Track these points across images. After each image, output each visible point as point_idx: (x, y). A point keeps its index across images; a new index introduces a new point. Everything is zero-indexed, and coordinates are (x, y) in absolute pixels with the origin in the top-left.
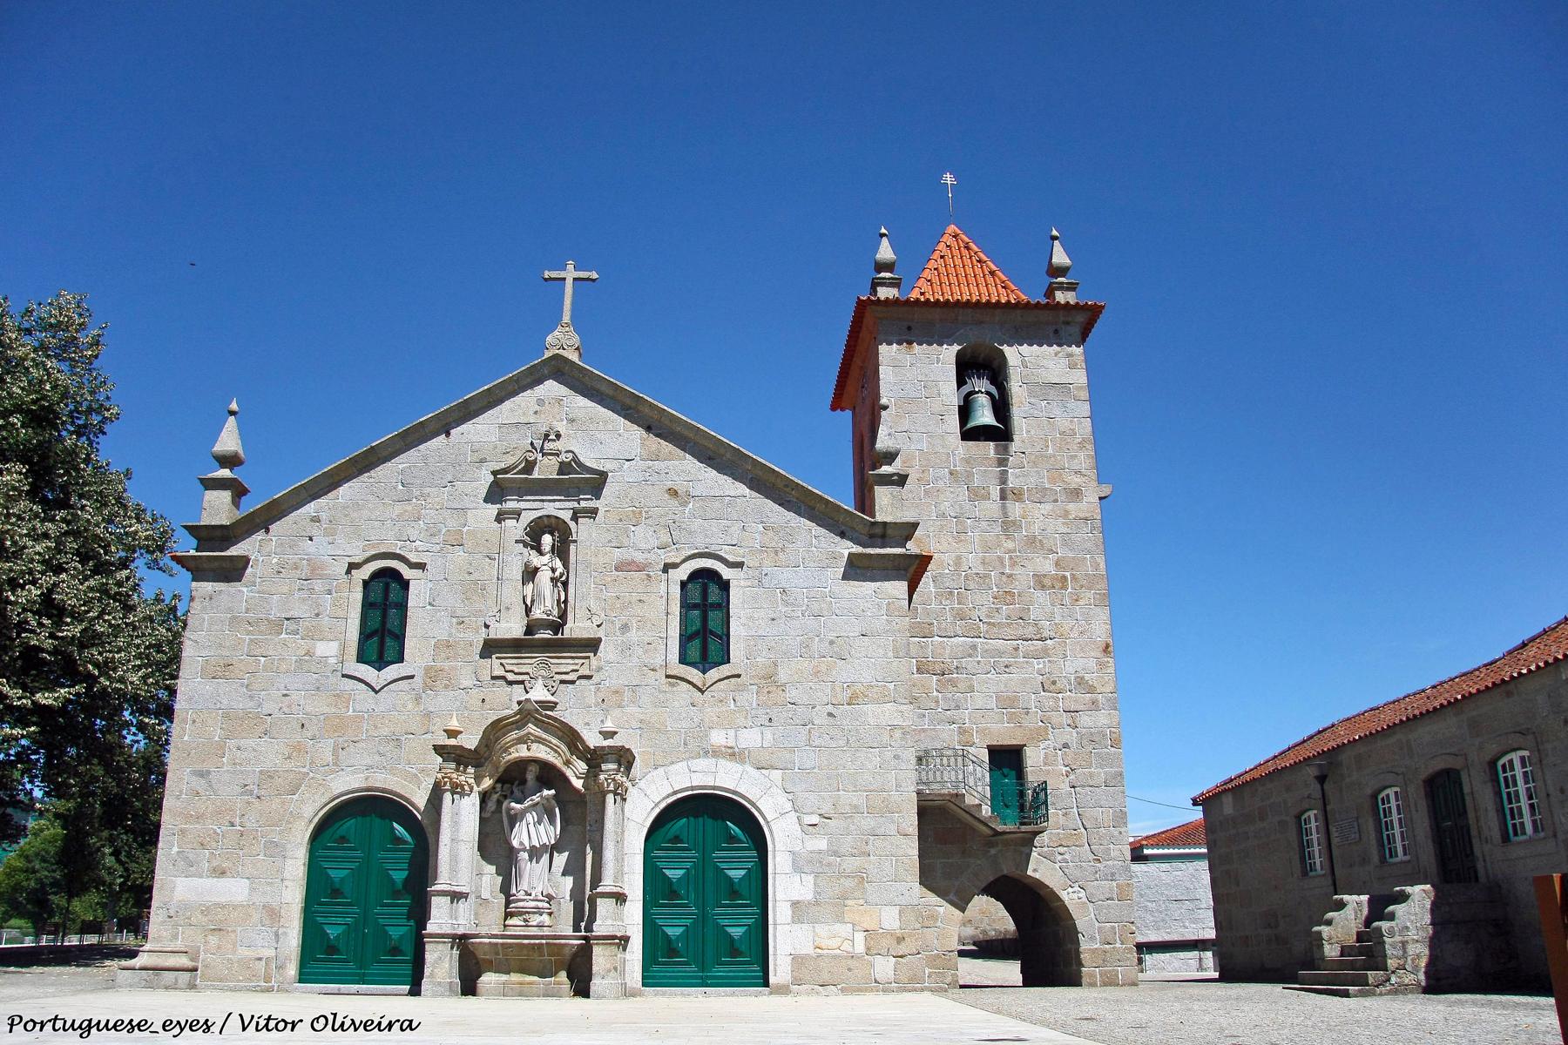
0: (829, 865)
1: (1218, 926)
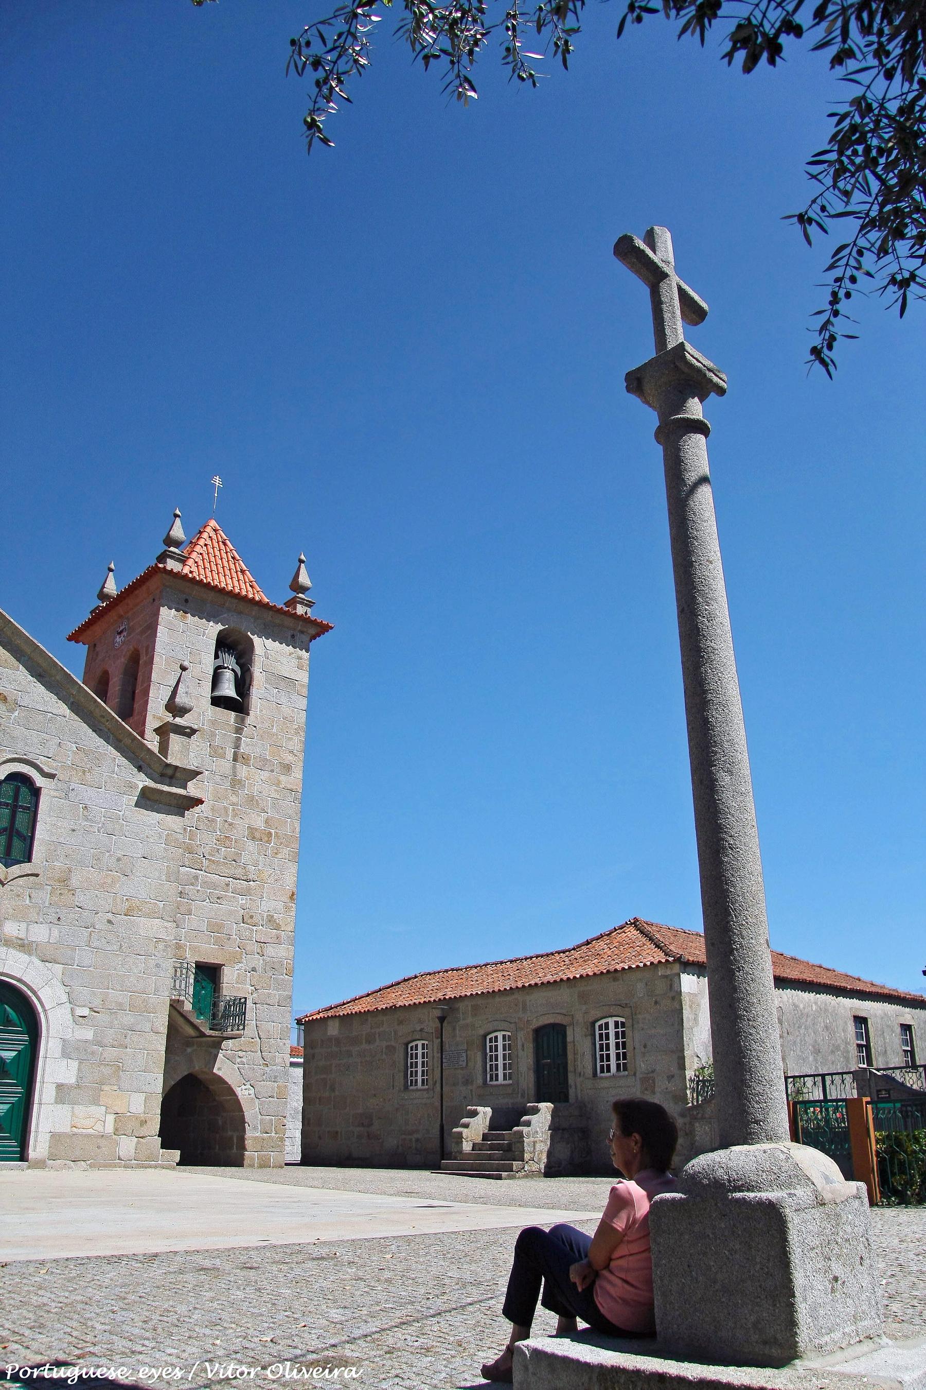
0: (93, 1053)
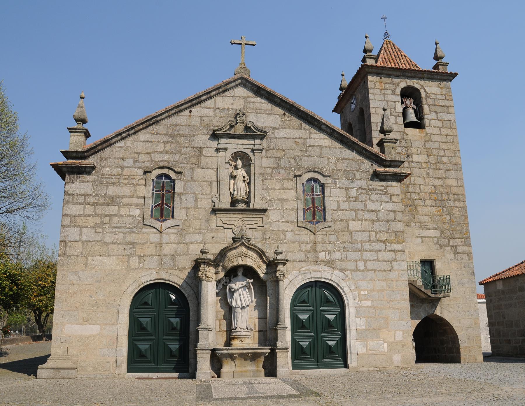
1: (493, 347)
